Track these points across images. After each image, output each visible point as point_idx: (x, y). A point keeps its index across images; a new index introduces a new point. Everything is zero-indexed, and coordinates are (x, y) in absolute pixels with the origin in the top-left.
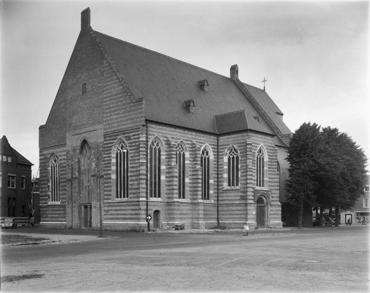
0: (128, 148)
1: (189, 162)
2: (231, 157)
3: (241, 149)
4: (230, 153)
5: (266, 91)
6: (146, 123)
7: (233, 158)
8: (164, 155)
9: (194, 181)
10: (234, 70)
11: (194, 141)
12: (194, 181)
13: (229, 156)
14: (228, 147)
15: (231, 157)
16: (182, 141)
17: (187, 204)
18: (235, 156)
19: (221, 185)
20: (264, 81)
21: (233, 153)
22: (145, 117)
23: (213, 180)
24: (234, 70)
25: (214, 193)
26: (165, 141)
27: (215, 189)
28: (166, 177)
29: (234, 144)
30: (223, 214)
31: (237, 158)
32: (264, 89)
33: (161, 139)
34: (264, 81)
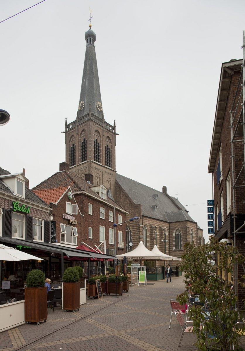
0: (131, 230)
1: (158, 236)
2: (177, 234)
3: (183, 230)
4: (176, 232)
5: (178, 199)
6: (142, 217)
7: (178, 235)
8: (149, 233)
9: (161, 246)
10: (165, 189)
11: (160, 226)
12: (161, 246)
13: (176, 234)
14: (176, 229)
15: (177, 234)
16: (155, 226)
17: (22, 234)
18: (179, 234)
19: (171, 248)
20: (177, 194)
21: (178, 232)
22: (28, 213)
23: (149, 244)
24: (165, 189)
25: (168, 252)
26: (149, 226)
27: (168, 250)
28: (150, 244)
29: (179, 227)
30: (173, 263)
31: (131, 232)
32: (177, 199)
33: (148, 225)
34: (177, 194)
